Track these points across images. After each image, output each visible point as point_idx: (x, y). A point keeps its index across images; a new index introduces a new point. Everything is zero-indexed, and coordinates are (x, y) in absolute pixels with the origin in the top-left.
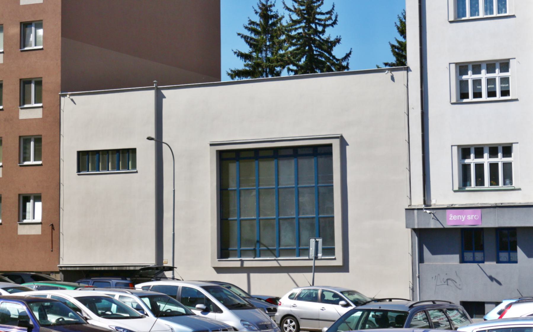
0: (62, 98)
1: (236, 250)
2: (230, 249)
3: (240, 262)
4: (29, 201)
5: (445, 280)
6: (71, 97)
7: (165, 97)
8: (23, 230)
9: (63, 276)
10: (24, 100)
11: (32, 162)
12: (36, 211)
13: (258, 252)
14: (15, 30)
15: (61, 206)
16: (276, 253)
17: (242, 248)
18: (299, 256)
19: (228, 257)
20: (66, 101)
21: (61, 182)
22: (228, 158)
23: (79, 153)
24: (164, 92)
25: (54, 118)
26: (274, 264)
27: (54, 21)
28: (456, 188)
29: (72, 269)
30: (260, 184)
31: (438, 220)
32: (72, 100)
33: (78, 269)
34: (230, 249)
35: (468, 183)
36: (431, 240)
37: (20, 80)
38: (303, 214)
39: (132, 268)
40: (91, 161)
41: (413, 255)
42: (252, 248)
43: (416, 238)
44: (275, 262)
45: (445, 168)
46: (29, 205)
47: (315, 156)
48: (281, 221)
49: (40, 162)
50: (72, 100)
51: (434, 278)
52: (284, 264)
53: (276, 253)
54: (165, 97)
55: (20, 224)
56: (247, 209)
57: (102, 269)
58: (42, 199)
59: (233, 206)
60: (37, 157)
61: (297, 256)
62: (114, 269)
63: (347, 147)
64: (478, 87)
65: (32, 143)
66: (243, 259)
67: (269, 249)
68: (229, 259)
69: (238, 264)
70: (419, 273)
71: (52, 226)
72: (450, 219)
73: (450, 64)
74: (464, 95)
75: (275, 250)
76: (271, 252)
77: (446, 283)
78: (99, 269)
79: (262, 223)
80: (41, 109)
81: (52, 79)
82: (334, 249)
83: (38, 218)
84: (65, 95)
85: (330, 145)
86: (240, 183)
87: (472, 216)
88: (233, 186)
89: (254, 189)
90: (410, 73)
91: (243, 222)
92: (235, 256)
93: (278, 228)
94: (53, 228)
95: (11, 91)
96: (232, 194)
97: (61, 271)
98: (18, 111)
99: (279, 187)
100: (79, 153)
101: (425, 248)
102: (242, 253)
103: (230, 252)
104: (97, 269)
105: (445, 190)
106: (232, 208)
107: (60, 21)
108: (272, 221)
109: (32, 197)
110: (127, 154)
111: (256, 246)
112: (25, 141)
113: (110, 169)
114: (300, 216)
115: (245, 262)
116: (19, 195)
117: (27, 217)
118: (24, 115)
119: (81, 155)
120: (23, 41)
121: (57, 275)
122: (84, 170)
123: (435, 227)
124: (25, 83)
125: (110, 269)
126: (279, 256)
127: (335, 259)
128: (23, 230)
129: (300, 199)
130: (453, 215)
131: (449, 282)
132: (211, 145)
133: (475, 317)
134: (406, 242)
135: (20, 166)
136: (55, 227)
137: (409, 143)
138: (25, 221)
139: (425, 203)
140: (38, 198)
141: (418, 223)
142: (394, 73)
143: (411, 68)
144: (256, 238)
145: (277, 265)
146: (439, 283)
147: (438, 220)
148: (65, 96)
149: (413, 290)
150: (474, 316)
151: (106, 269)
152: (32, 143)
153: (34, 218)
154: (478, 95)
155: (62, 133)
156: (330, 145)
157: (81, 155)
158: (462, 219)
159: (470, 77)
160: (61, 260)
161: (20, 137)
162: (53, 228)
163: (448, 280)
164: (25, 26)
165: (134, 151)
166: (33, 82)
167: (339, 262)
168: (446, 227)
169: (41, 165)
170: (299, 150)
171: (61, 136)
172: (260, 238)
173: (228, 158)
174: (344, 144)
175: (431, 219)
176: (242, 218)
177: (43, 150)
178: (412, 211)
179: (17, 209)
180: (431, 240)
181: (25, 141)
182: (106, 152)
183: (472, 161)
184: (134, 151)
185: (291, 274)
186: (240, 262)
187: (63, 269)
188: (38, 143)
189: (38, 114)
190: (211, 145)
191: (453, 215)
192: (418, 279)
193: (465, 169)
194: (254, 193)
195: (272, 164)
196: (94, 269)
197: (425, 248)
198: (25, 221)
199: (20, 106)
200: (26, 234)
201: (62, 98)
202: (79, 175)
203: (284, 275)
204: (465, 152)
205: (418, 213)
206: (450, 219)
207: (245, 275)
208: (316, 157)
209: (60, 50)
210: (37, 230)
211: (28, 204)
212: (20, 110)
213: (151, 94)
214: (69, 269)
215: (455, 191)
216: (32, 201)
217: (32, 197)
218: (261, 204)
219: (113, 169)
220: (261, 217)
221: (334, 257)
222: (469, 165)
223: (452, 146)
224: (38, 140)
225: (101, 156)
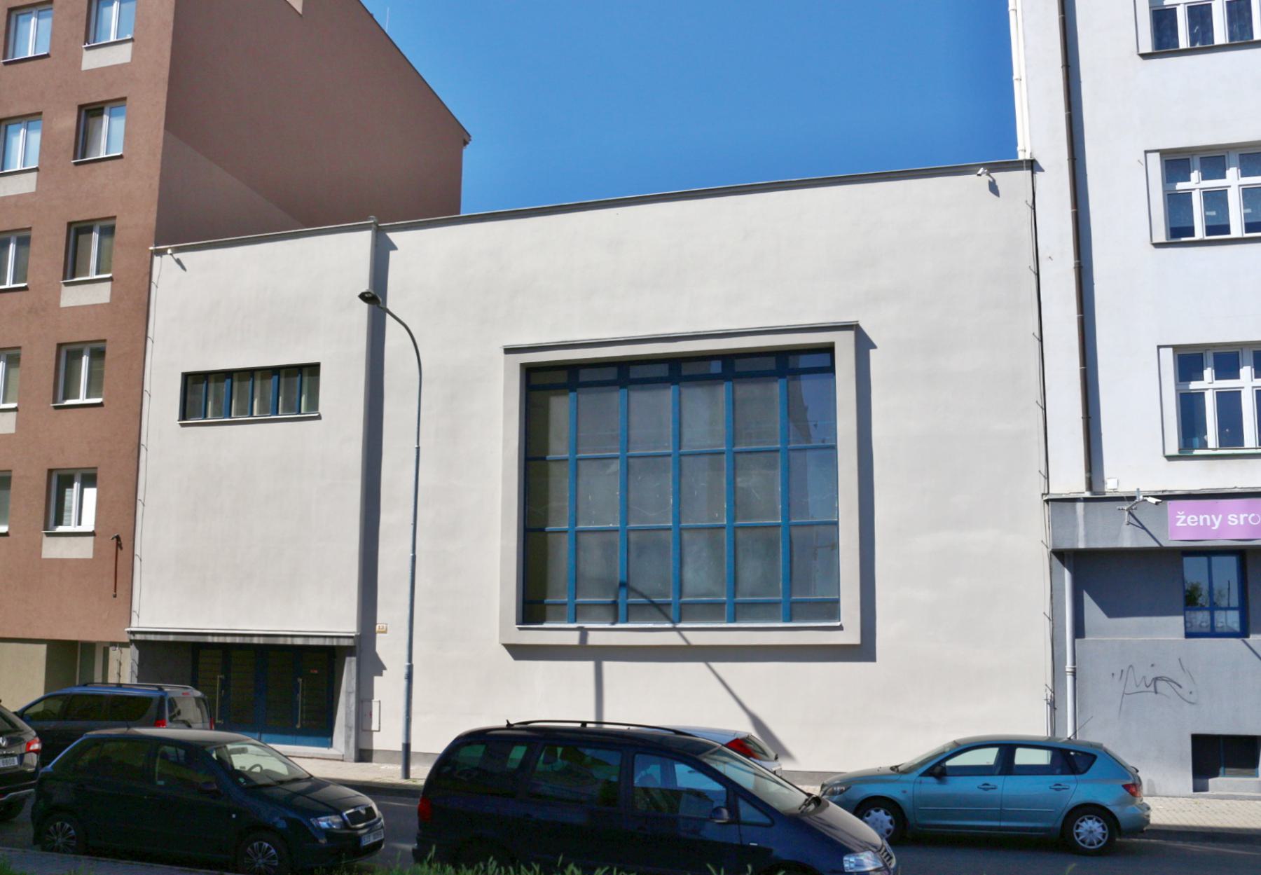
0: (157, 259)
1: (564, 604)
2: (548, 600)
3: (577, 634)
4: (71, 486)
5: (1149, 681)
6: (177, 256)
7: (395, 248)
8: (54, 549)
10: (72, 268)
12: (85, 507)
13: (622, 610)
14: (68, 122)
15: (140, 496)
16: (673, 612)
17: (580, 600)
18: (735, 620)
19: (542, 622)
20: (164, 266)
21: (143, 441)
22: (548, 383)
23: (186, 376)
24: (394, 237)
25: (136, 304)
26: (672, 639)
28: (1173, 449)
29: (159, 638)
30: (580, 448)
31: (1144, 528)
32: (178, 261)
33: (171, 638)
34: (548, 600)
35: (1196, 441)
36: (1110, 576)
37: (70, 224)
38: (744, 518)
39: (299, 641)
40: (206, 394)
41: (1055, 617)
43: (1067, 575)
44: (675, 634)
46: (72, 494)
48: (740, 533)
49: (98, 400)
50: (178, 261)
51: (1117, 676)
52: (697, 639)
53: (673, 612)
54: (395, 248)
55: (48, 535)
56: (594, 501)
57: (229, 640)
58: (98, 481)
59: (559, 500)
62: (256, 640)
63: (392, 253)
65: (85, 360)
66: (587, 626)
67: (653, 604)
68: (545, 625)
69: (573, 639)
70: (1074, 663)
71: (118, 543)
72: (1179, 524)
75: (669, 604)
76: (657, 609)
77: (1152, 688)
78: (221, 640)
79: (633, 541)
80: (109, 284)
81: (138, 218)
83: (88, 524)
84: (163, 252)
85: (829, 349)
86: (576, 445)
87: (1242, 516)
88: (558, 447)
89: (616, 458)
90: (1038, 175)
91: (583, 537)
92: (560, 618)
94: (119, 545)
95: (49, 247)
96: (554, 469)
97: (132, 641)
98: (60, 290)
100: (186, 376)
101: (1088, 600)
102: (578, 612)
104: (216, 640)
105: (1141, 457)
106: (553, 504)
107: (165, 95)
108: (663, 534)
109: (78, 477)
110: (298, 379)
111: (617, 596)
112: (68, 354)
113: (255, 413)
115: (591, 634)
116: (50, 471)
118: (72, 297)
119: (194, 383)
120: (83, 141)
121: (124, 650)
122: (193, 416)
123: (1135, 545)
124: (78, 231)
126: (680, 621)
127: (840, 628)
128: (54, 549)
129: (739, 480)
130: (1187, 515)
131: (1160, 684)
134: (1034, 587)
135: (56, 408)
136: (124, 542)
137: (1041, 341)
138: (60, 529)
140: (89, 479)
141: (1086, 535)
142: (997, 176)
143: (1042, 163)
144: (619, 576)
145: (681, 642)
146: (1131, 688)
147: (1144, 528)
148: (161, 253)
151: (238, 640)
152: (85, 360)
153: (79, 524)
155: (150, 334)
156: (829, 349)
157: (194, 383)
158: (1213, 524)
160: (134, 616)
161: (60, 346)
162: (119, 545)
163: (1156, 679)
164: (91, 112)
165: (314, 369)
166: (97, 228)
167: (851, 635)
168: (701, 665)
169: (100, 405)
170: (738, 362)
171: (149, 342)
173: (548, 383)
174: (864, 345)
176: (581, 526)
177: (106, 373)
178: (1069, 505)
179: (43, 502)
180: (1110, 576)
181: (68, 354)
182: (249, 373)
183: (1208, 384)
184: (314, 369)
185: (714, 665)
187: (138, 637)
188: (94, 359)
189: (100, 294)
190: (508, 351)
191: (1187, 515)
192: (1069, 679)
193: (1190, 408)
194: (616, 466)
195: (667, 396)
196: (210, 639)
198: (60, 529)
199: (64, 278)
200: (59, 557)
202: (182, 425)
203: (698, 668)
204: (1189, 361)
205: (1085, 509)
206: (1179, 524)
207: (590, 665)
208: (782, 381)
209: (159, 157)
210: (83, 550)
211: (68, 491)
212: (63, 287)
213: (364, 239)
214: (152, 638)
215: (1170, 458)
216: (76, 485)
217: (78, 477)
218: (632, 496)
219: (215, 415)
220: (632, 525)
223: (1159, 347)
224: (98, 354)
225: (236, 384)
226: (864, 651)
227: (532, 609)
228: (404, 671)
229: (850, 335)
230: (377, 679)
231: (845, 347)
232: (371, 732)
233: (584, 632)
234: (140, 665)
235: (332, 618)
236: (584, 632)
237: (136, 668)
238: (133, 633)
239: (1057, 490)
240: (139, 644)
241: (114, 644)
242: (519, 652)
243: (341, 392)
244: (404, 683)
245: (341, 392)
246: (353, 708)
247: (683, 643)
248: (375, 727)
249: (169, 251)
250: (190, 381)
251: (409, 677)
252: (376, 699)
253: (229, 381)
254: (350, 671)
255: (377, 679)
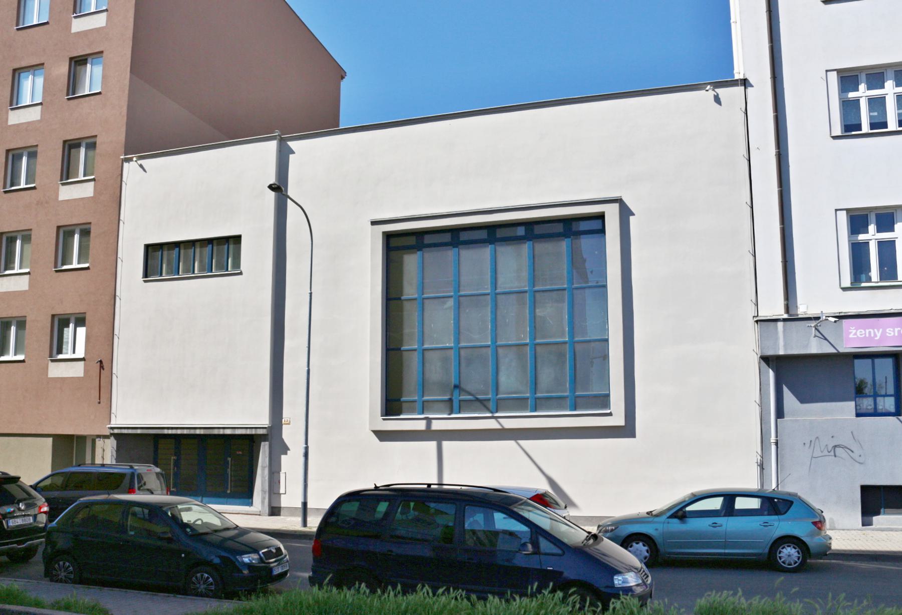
0: (126, 165)
3: (424, 422)
4: (68, 326)
5: (830, 448)
6: (140, 162)
8: (56, 371)
9: (115, 442)
10: (67, 173)
11: (75, 265)
12: (78, 340)
13: (456, 404)
16: (491, 405)
20: (131, 169)
21: (118, 293)
22: (401, 244)
23: (148, 247)
25: (112, 198)
26: (492, 424)
27: (120, 53)
29: (130, 431)
31: (826, 339)
32: (141, 166)
33: (139, 431)
34: (403, 399)
35: (863, 277)
36: (797, 375)
38: (543, 338)
39: (228, 432)
40: (162, 259)
42: (446, 398)
43: (771, 374)
44: (493, 420)
45: (823, 251)
46: (69, 332)
47: (566, 237)
50: (141, 166)
51: (808, 445)
52: (509, 424)
55: (52, 361)
57: (179, 432)
60: (82, 257)
61: (531, 411)
62: (198, 432)
63: (631, 218)
64: (876, 114)
65: (77, 237)
67: (478, 400)
68: (402, 417)
69: (421, 426)
72: (851, 336)
73: (827, 71)
74: (851, 128)
76: (481, 404)
77: (832, 453)
81: (112, 136)
82: (608, 396)
83: (80, 353)
84: (130, 160)
87: (896, 330)
88: (410, 291)
89: (451, 297)
90: (749, 89)
91: (427, 354)
92: (412, 411)
93: (470, 232)
94: (102, 367)
96: (407, 306)
97: (112, 434)
98: (58, 189)
99: (497, 291)
100: (148, 247)
101: (786, 392)
103: (405, 406)
104: (170, 432)
105: (824, 288)
108: (484, 350)
109: (73, 319)
110: (226, 246)
111: (452, 395)
112: (65, 233)
113: (196, 272)
114: (538, 341)
116: (53, 316)
117: (64, 351)
118: (67, 193)
119: (150, 249)
121: (106, 440)
123: (820, 352)
124: (71, 146)
125: (192, 432)
126: (497, 412)
127: (610, 414)
129: (537, 310)
132: (374, 223)
133: (884, 514)
134: (749, 383)
135: (57, 271)
136: (105, 364)
137: (752, 208)
138: (60, 357)
139: (787, 310)
140: (81, 321)
141: (785, 346)
143: (751, 81)
145: (499, 427)
147: (826, 339)
148: (128, 160)
149: (762, 466)
150: (882, 510)
151: (185, 432)
152: (77, 237)
153: (74, 352)
154: (879, 125)
158: (875, 335)
159: (863, 93)
162: (102, 367)
164: (79, 62)
165: (237, 239)
167: (618, 419)
168: (842, 350)
171: (121, 223)
172: (460, 382)
173: (401, 244)
174: (625, 213)
175: (812, 338)
176: (426, 346)
179: (49, 338)
180: (797, 375)
181: (65, 233)
183: (872, 236)
184: (237, 239)
185: (521, 442)
186: (424, 422)
187: (116, 431)
188: (81, 237)
189: (87, 191)
190: (374, 223)
192: (773, 447)
193: (859, 253)
194: (450, 303)
195: (486, 252)
196: (166, 432)
197: (786, 392)
198: (60, 357)
201: (126, 165)
202: (145, 281)
203: (509, 445)
205: (784, 326)
206: (851, 336)
207: (433, 444)
209: (127, 92)
210: (77, 371)
214: (125, 431)
216: (72, 326)
220: (463, 344)
221: (609, 411)
222: (866, 244)
224: (85, 233)
226: (627, 430)
227: (392, 405)
228: (303, 451)
229: (616, 207)
230: (283, 457)
231: (612, 214)
232: (280, 494)
233: (429, 421)
234: (118, 451)
235: (255, 416)
236: (429, 421)
237: (115, 453)
238: (112, 428)
239: (764, 313)
240: (117, 436)
241: (99, 436)
242: (382, 436)
243: (256, 255)
244: (302, 459)
245: (256, 255)
246: (267, 478)
247: (499, 427)
248: (282, 491)
249: (135, 159)
250: (150, 250)
251: (306, 455)
252: (283, 471)
253: (177, 249)
254: (264, 452)
255: (283, 457)
